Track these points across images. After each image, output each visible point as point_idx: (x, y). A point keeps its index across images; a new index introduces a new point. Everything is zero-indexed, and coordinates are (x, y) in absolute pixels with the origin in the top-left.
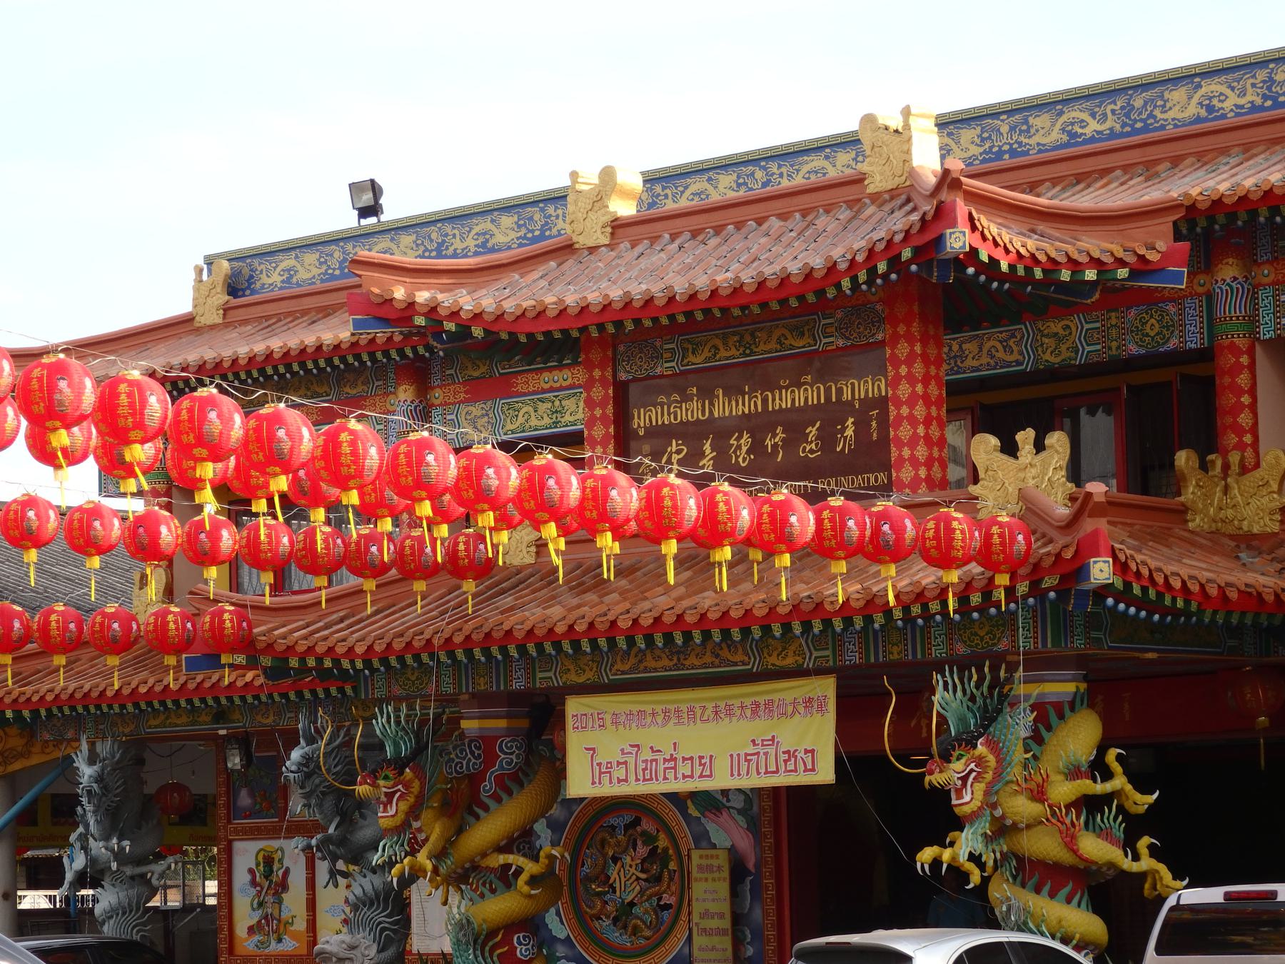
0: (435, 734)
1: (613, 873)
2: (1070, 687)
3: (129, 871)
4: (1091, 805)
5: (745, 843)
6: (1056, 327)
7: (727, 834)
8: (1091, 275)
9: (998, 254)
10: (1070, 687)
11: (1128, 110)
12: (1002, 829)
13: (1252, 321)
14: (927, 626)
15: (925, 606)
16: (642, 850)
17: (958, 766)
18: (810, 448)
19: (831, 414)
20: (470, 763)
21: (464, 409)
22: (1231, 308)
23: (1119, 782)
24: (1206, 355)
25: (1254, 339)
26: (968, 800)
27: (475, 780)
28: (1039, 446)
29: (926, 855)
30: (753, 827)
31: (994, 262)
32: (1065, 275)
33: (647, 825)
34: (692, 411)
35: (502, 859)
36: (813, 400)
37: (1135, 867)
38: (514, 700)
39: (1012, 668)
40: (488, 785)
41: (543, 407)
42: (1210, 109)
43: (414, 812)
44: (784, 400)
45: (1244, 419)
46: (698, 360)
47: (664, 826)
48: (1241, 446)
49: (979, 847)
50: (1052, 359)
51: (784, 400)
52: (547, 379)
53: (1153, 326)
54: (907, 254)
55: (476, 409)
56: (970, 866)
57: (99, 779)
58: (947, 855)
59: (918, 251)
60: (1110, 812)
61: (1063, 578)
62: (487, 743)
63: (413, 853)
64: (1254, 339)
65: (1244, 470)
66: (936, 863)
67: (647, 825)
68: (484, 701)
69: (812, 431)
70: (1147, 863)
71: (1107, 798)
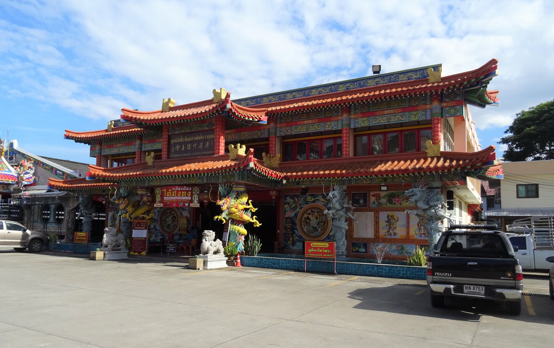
0: (131, 193)
1: (167, 219)
2: (243, 189)
3: (88, 216)
4: (246, 210)
5: (188, 215)
6: (243, 133)
7: (186, 214)
8: (251, 119)
9: (236, 112)
10: (243, 189)
11: (257, 101)
12: (230, 213)
13: (276, 133)
14: (218, 176)
15: (218, 172)
16: (172, 216)
17: (223, 201)
18: (201, 146)
19: (205, 141)
20: (138, 198)
21: (360, 119)
22: (272, 131)
23: (251, 206)
24: (267, 139)
25: (276, 136)
26: (224, 208)
27: (139, 202)
28: (241, 147)
29: (216, 217)
30: (190, 213)
31: (235, 113)
32: (247, 118)
33: (173, 212)
34: (181, 140)
35: (143, 215)
36: (202, 138)
37: (253, 221)
38: (147, 188)
39: (233, 185)
40: (141, 203)
41: (384, 118)
42: (270, 101)
43: (126, 206)
44: (197, 138)
45: (274, 149)
46: (183, 131)
47: (176, 212)
48: (273, 153)
49: (225, 216)
50: (414, 120)
51: (197, 138)
52: (305, 122)
53: (259, 134)
54: (219, 109)
55: (149, 145)
56: (224, 220)
57: (83, 201)
58: (220, 217)
59: (221, 109)
60: (249, 211)
61: (244, 166)
62: (142, 196)
63: (126, 213)
64: (276, 136)
65: (273, 157)
66: (218, 219)
67: (173, 212)
68: (142, 188)
69: (201, 144)
70: (255, 221)
71: (248, 209)
